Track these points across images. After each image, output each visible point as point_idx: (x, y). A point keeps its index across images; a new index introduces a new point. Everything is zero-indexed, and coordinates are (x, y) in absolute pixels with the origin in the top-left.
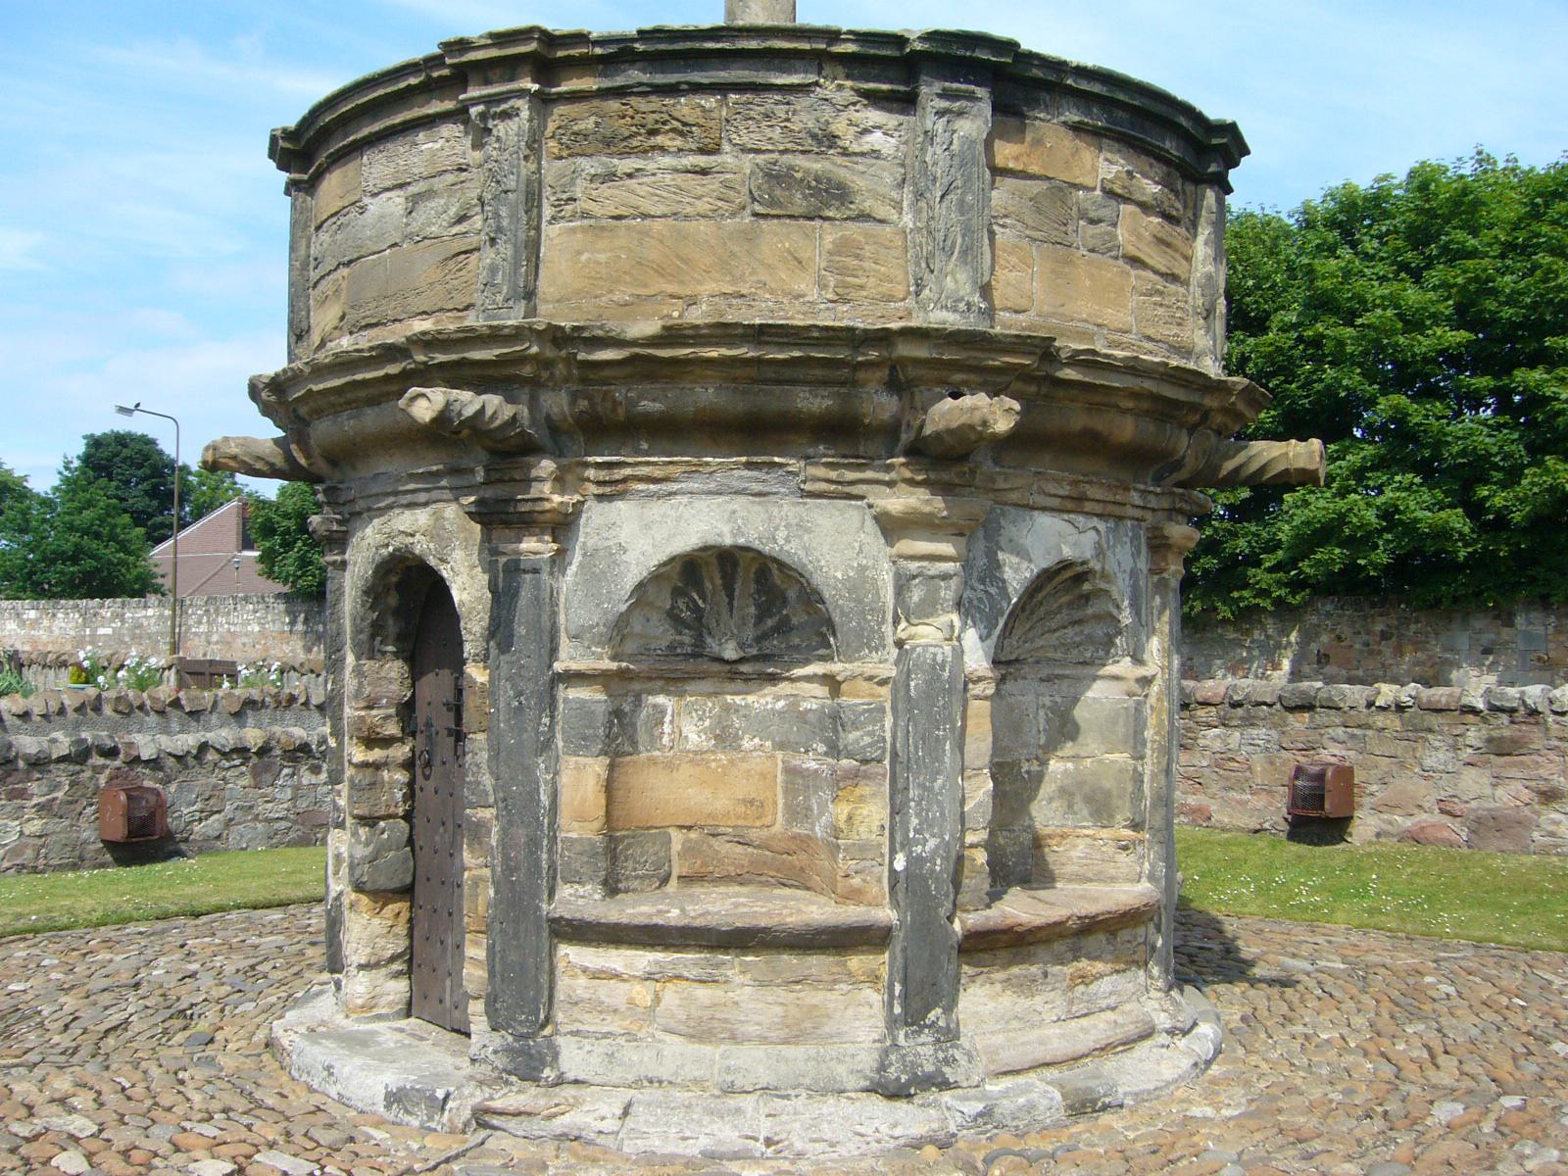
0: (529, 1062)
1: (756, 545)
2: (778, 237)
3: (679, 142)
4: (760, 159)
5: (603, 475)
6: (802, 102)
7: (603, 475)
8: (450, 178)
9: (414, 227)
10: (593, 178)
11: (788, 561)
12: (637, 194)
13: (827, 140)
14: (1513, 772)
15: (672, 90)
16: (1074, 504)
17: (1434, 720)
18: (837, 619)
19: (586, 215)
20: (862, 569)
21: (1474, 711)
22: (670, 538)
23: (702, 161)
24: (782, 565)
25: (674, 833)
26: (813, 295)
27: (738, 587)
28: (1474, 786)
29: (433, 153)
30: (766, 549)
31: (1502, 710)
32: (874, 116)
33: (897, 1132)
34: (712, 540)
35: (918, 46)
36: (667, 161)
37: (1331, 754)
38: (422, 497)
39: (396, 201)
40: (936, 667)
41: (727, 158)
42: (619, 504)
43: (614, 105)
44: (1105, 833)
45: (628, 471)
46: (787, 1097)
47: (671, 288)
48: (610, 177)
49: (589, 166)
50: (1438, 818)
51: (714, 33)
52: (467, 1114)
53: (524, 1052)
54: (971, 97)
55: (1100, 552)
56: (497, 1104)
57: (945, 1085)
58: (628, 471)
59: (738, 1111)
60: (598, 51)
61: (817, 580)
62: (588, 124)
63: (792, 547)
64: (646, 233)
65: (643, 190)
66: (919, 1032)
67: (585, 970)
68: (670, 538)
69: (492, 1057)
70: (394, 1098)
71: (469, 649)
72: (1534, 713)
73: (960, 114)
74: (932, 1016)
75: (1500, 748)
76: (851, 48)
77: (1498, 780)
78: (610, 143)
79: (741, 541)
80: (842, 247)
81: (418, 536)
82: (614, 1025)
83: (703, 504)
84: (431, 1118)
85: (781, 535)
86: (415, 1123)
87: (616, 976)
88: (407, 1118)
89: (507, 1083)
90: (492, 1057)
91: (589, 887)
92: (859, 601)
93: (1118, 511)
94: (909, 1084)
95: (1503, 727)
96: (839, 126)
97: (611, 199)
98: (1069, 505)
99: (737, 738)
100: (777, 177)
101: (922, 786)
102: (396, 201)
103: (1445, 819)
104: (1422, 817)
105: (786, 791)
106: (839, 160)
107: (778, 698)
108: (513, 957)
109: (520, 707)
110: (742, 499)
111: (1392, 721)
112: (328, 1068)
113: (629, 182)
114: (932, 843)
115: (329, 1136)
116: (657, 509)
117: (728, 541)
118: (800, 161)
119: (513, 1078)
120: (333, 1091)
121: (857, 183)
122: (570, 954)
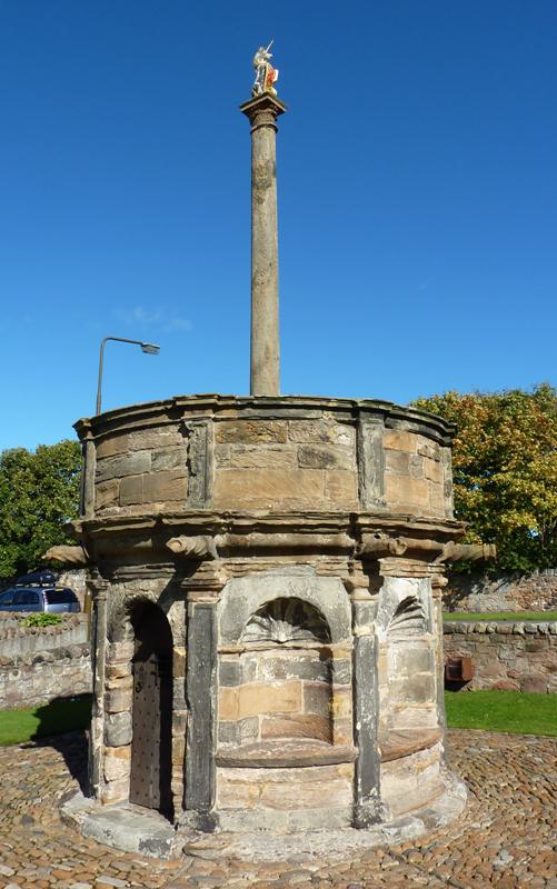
0: (208, 824)
1: (299, 596)
2: (309, 476)
3: (270, 438)
4: (302, 446)
5: (238, 568)
6: (316, 424)
7: (238, 568)
8: (174, 448)
9: (156, 466)
10: (236, 451)
11: (312, 603)
12: (255, 459)
13: (326, 439)
14: (538, 660)
15: (267, 419)
16: (411, 574)
17: (503, 638)
18: (331, 626)
19: (232, 466)
20: (340, 605)
21: (519, 634)
22: (265, 594)
23: (279, 446)
24: (309, 605)
25: (259, 716)
26: (322, 498)
27: (287, 611)
28: (522, 665)
29: (165, 437)
30: (303, 598)
31: (531, 633)
32: (343, 429)
33: (365, 845)
34: (282, 595)
35: (360, 405)
36: (266, 446)
37: (462, 652)
38: (154, 576)
39: (148, 455)
40: (369, 644)
41: (289, 445)
42: (243, 580)
43: (244, 423)
44: (422, 705)
45: (248, 567)
46: (317, 832)
47: (269, 496)
48: (243, 451)
49: (235, 447)
50: (506, 679)
51: (284, 399)
52: (180, 850)
53: (206, 819)
54: (377, 423)
55: (419, 592)
56: (196, 845)
57: (380, 821)
58: (248, 567)
59: (299, 841)
60: (239, 403)
61: (323, 610)
62: (234, 430)
63: (313, 597)
64: (258, 474)
65: (256, 457)
66: (368, 799)
67: (229, 780)
68: (265, 594)
69: (190, 823)
70: (143, 845)
71: (175, 641)
72: (542, 634)
73: (374, 429)
74: (372, 791)
75: (531, 649)
76: (335, 405)
77: (532, 663)
78: (242, 438)
79: (294, 595)
80: (333, 480)
81: (150, 592)
82: (242, 805)
83: (278, 580)
84: (164, 853)
85: (309, 592)
86: (155, 856)
87: (244, 782)
88: (151, 854)
89: (198, 835)
90: (190, 823)
91: (231, 744)
92: (339, 618)
93: (423, 575)
94: (367, 822)
95: (532, 640)
96: (330, 434)
97: (241, 461)
98: (410, 574)
99: (284, 674)
100: (309, 453)
101: (365, 693)
102: (148, 455)
103: (511, 679)
104: (499, 679)
105: (305, 696)
106: (331, 447)
107: (301, 657)
108: (198, 777)
109: (202, 667)
110: (294, 578)
111: (486, 639)
112: (107, 832)
113: (252, 454)
114: (370, 717)
115: (126, 869)
116: (260, 583)
117: (288, 595)
118: (317, 447)
119: (201, 832)
120: (110, 843)
121: (337, 455)
122: (221, 772)
